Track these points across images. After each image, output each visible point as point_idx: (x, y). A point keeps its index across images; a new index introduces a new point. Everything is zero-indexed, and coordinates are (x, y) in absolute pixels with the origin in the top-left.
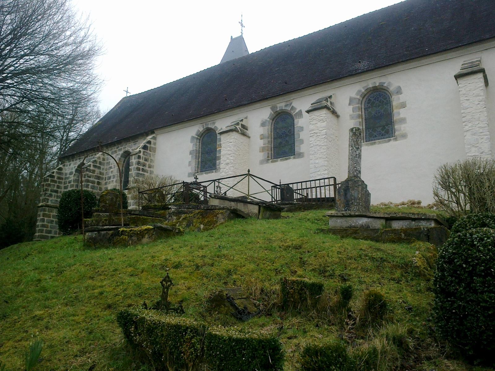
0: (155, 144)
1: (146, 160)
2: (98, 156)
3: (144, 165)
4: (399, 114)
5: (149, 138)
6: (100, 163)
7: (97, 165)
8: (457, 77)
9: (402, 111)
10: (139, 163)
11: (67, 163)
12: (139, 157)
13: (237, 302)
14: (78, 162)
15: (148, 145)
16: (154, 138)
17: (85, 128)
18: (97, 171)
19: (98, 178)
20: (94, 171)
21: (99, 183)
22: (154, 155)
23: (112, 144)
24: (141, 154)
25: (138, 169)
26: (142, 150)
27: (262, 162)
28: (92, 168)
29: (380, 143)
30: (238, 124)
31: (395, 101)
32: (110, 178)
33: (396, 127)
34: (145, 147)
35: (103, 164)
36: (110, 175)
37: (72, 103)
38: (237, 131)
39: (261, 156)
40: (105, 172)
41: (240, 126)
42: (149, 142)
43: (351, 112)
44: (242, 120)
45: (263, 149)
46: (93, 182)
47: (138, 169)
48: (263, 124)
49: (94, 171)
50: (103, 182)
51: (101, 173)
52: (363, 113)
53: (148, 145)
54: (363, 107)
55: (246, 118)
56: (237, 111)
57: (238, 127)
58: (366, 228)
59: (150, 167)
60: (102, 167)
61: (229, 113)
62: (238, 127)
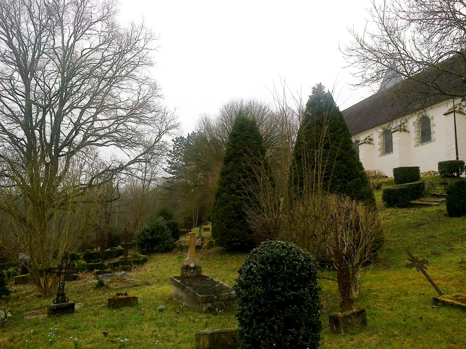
4: (433, 129)
8: (445, 114)
9: (434, 128)
17: (294, 138)
27: (379, 156)
29: (425, 144)
30: (366, 139)
31: (432, 122)
33: (432, 136)
38: (366, 143)
39: (379, 153)
41: (368, 140)
43: (414, 130)
44: (369, 136)
45: (416, 139)
52: (420, 129)
54: (420, 126)
56: (368, 131)
57: (366, 141)
58: (31, 114)
61: (365, 132)
62: (366, 141)
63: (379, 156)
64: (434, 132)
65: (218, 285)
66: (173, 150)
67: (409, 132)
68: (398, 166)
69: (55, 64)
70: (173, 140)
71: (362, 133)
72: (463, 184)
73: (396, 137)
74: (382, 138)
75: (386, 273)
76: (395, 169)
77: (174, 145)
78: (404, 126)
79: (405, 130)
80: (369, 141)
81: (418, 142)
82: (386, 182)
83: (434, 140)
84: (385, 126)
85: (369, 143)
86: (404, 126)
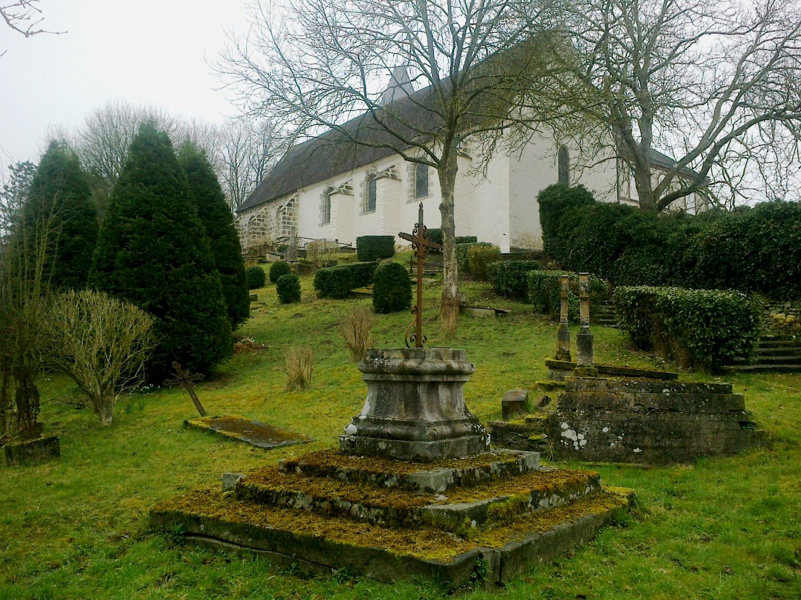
0: (298, 200)
1: (290, 215)
2: (261, 211)
3: (289, 219)
5: (293, 197)
6: (263, 217)
7: (261, 219)
10: (284, 218)
11: (242, 216)
12: (284, 213)
13: (715, 169)
14: (250, 215)
15: (292, 202)
16: (297, 196)
18: (261, 223)
19: (263, 229)
20: (259, 224)
21: (263, 234)
22: (297, 210)
23: (270, 201)
24: (286, 211)
25: (284, 223)
26: (287, 207)
27: (360, 215)
28: (257, 222)
30: (342, 187)
32: (271, 229)
33: (429, 188)
34: (289, 205)
35: (266, 217)
36: (272, 226)
37: (665, 65)
39: (359, 209)
40: (268, 223)
41: (344, 188)
42: (293, 200)
46: (259, 233)
47: (284, 223)
48: (361, 186)
49: (259, 224)
50: (267, 232)
51: (264, 225)
53: (292, 202)
55: (351, 180)
57: (341, 189)
59: (294, 220)
60: (265, 220)
62: (341, 189)
63: (360, 215)
64: (432, 183)
65: (673, 302)
66: (10, 185)
67: (400, 180)
68: (362, 234)
69: (691, 105)
70: (11, 167)
71: (337, 177)
72: (395, 268)
73: (381, 186)
74: (365, 187)
75: (234, 416)
76: (359, 238)
77: (13, 175)
78: (393, 171)
79: (394, 177)
80: (347, 190)
81: (411, 196)
82: (347, 259)
83: (432, 195)
84: (369, 167)
85: (346, 193)
86: (393, 171)
